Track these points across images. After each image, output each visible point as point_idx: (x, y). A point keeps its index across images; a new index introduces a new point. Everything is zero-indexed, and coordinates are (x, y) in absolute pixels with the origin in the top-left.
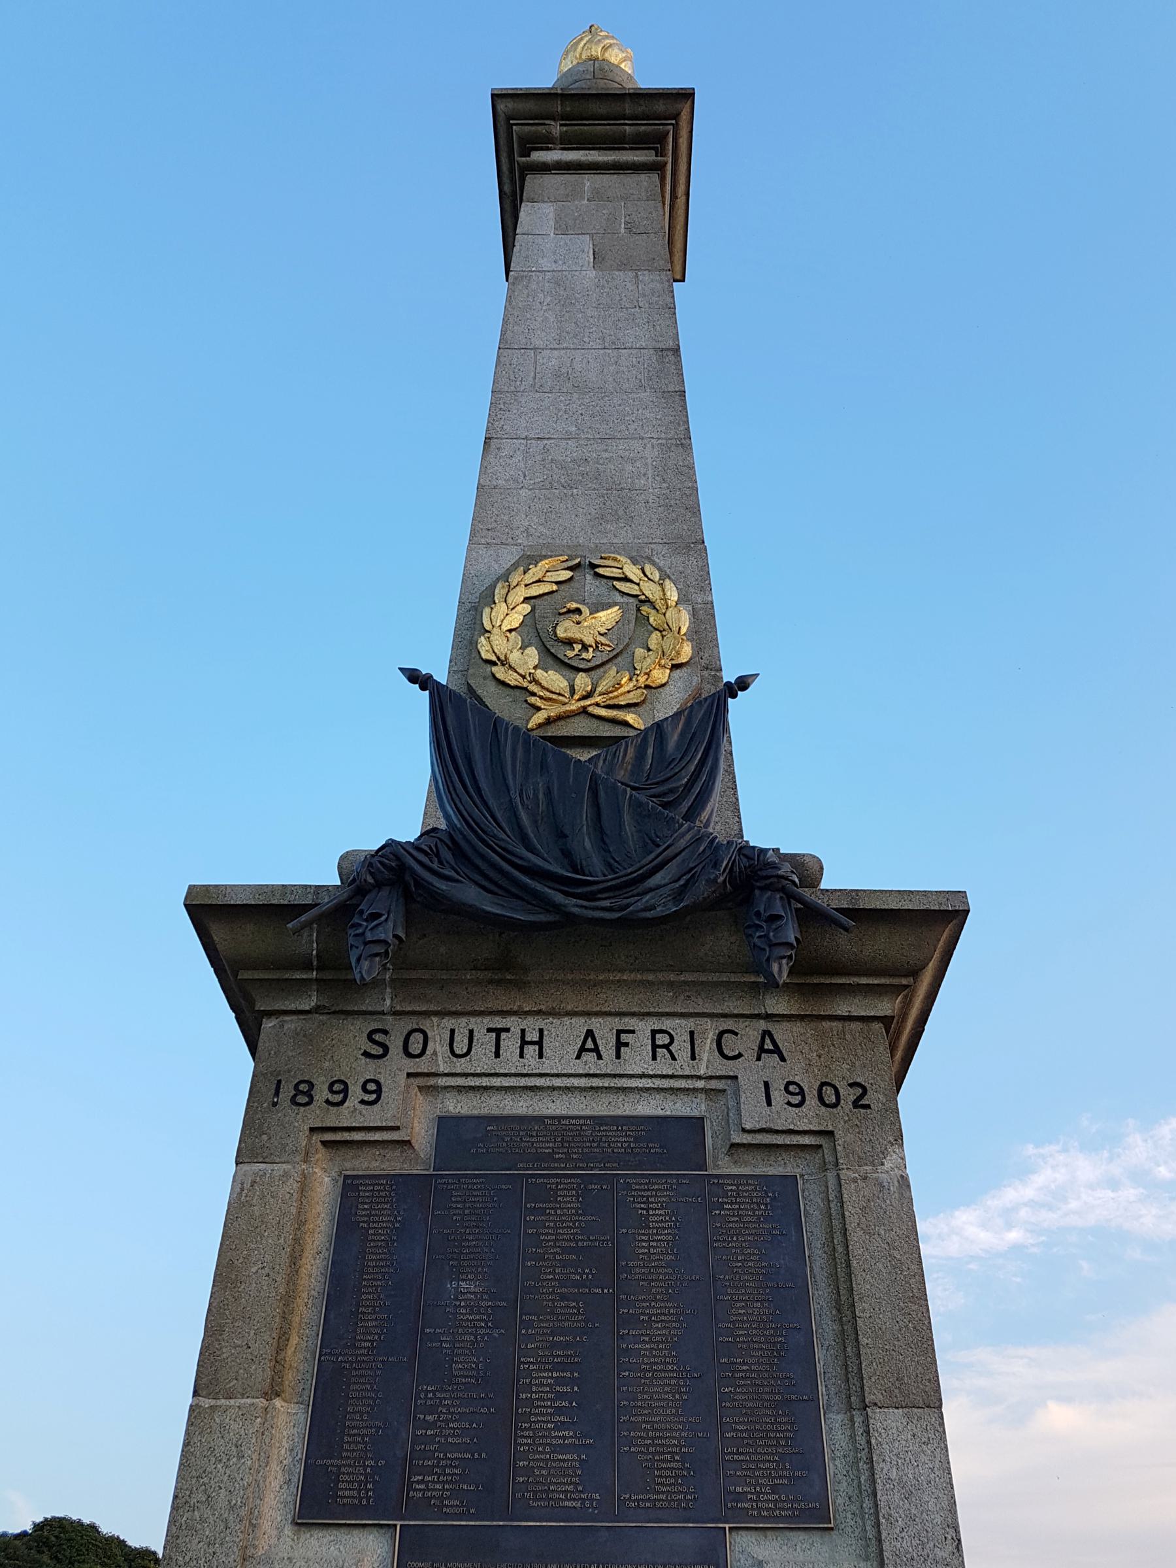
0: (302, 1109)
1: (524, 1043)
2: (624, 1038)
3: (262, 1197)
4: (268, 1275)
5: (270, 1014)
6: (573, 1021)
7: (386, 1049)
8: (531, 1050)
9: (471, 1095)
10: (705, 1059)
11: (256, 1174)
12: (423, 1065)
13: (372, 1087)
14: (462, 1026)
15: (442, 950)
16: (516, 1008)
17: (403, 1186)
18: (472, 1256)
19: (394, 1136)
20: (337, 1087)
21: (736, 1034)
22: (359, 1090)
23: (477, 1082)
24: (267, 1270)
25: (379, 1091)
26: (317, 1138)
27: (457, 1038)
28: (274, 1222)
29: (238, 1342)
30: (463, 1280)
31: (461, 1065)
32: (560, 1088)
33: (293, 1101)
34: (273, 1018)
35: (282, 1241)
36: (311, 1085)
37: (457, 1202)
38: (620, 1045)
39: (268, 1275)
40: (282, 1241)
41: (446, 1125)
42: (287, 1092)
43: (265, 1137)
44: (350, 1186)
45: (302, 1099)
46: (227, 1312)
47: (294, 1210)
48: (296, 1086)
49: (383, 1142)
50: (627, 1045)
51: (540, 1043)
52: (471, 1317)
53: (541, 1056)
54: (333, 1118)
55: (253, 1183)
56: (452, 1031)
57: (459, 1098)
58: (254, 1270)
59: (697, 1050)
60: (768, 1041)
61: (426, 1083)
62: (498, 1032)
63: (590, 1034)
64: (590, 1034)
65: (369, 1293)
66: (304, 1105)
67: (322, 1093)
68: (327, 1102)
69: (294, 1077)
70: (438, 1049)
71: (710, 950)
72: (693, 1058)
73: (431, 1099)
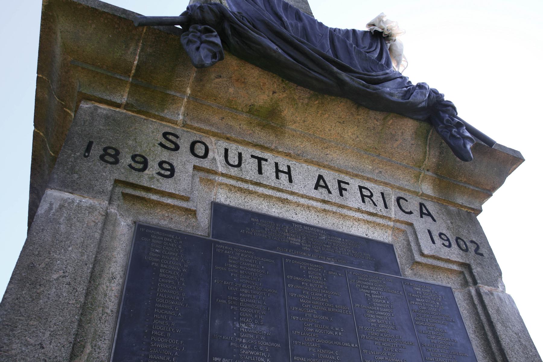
0: (109, 165)
1: (278, 171)
2: (343, 185)
3: (69, 219)
4: (69, 284)
5: (88, 98)
6: (309, 167)
7: (177, 148)
8: (284, 177)
9: (238, 195)
10: (393, 209)
11: (65, 201)
12: (205, 164)
13: (166, 166)
14: (234, 150)
15: (231, 90)
16: (273, 147)
17: (185, 241)
18: (248, 305)
19: (184, 205)
20: (138, 159)
21: (407, 201)
22: (156, 166)
23: (245, 186)
24: (68, 280)
25: (172, 170)
26: (119, 190)
27: (230, 155)
28: (79, 241)
29: (32, 341)
30: (243, 322)
31: (233, 171)
32: (303, 205)
33: (102, 158)
34: (89, 102)
35: (85, 258)
36: (117, 152)
37: (233, 264)
38: (341, 190)
39: (69, 284)
40: (85, 258)
41: (218, 209)
42: (97, 151)
43: (76, 176)
44: (143, 233)
45: (112, 152)
46: (22, 310)
47: (97, 236)
48: (105, 149)
49: (173, 206)
50: (346, 190)
51: (289, 173)
52: (252, 353)
53: (291, 181)
54: (133, 178)
55: (61, 207)
56: (226, 151)
57: (229, 195)
58: (55, 276)
59: (388, 203)
60: (424, 209)
61: (206, 174)
62: (260, 160)
63: (320, 177)
64: (320, 177)
65: (161, 319)
66: (111, 163)
67: (126, 160)
68: (130, 166)
69: (104, 142)
70: (217, 157)
71: (400, 144)
72: (386, 207)
73: (354, 110)
